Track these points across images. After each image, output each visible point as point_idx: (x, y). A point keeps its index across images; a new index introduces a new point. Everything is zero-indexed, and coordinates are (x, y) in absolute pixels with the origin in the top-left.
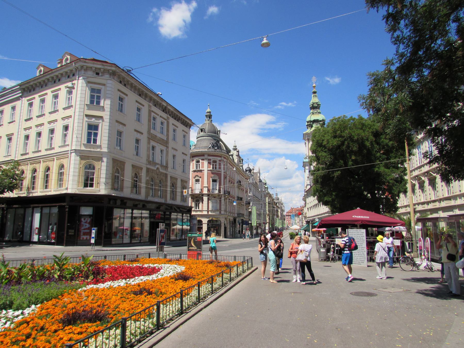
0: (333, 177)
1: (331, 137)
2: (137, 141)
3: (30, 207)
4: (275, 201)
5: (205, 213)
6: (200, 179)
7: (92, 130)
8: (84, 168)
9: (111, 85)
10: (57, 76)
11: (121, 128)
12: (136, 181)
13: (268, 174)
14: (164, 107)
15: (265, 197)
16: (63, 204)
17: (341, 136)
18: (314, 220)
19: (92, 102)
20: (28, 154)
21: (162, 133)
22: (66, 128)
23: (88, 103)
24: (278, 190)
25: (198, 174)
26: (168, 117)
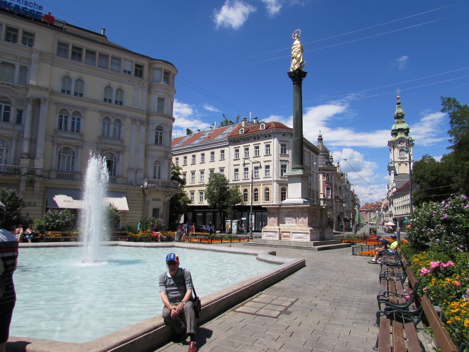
17: (436, 175)
19: (282, 152)
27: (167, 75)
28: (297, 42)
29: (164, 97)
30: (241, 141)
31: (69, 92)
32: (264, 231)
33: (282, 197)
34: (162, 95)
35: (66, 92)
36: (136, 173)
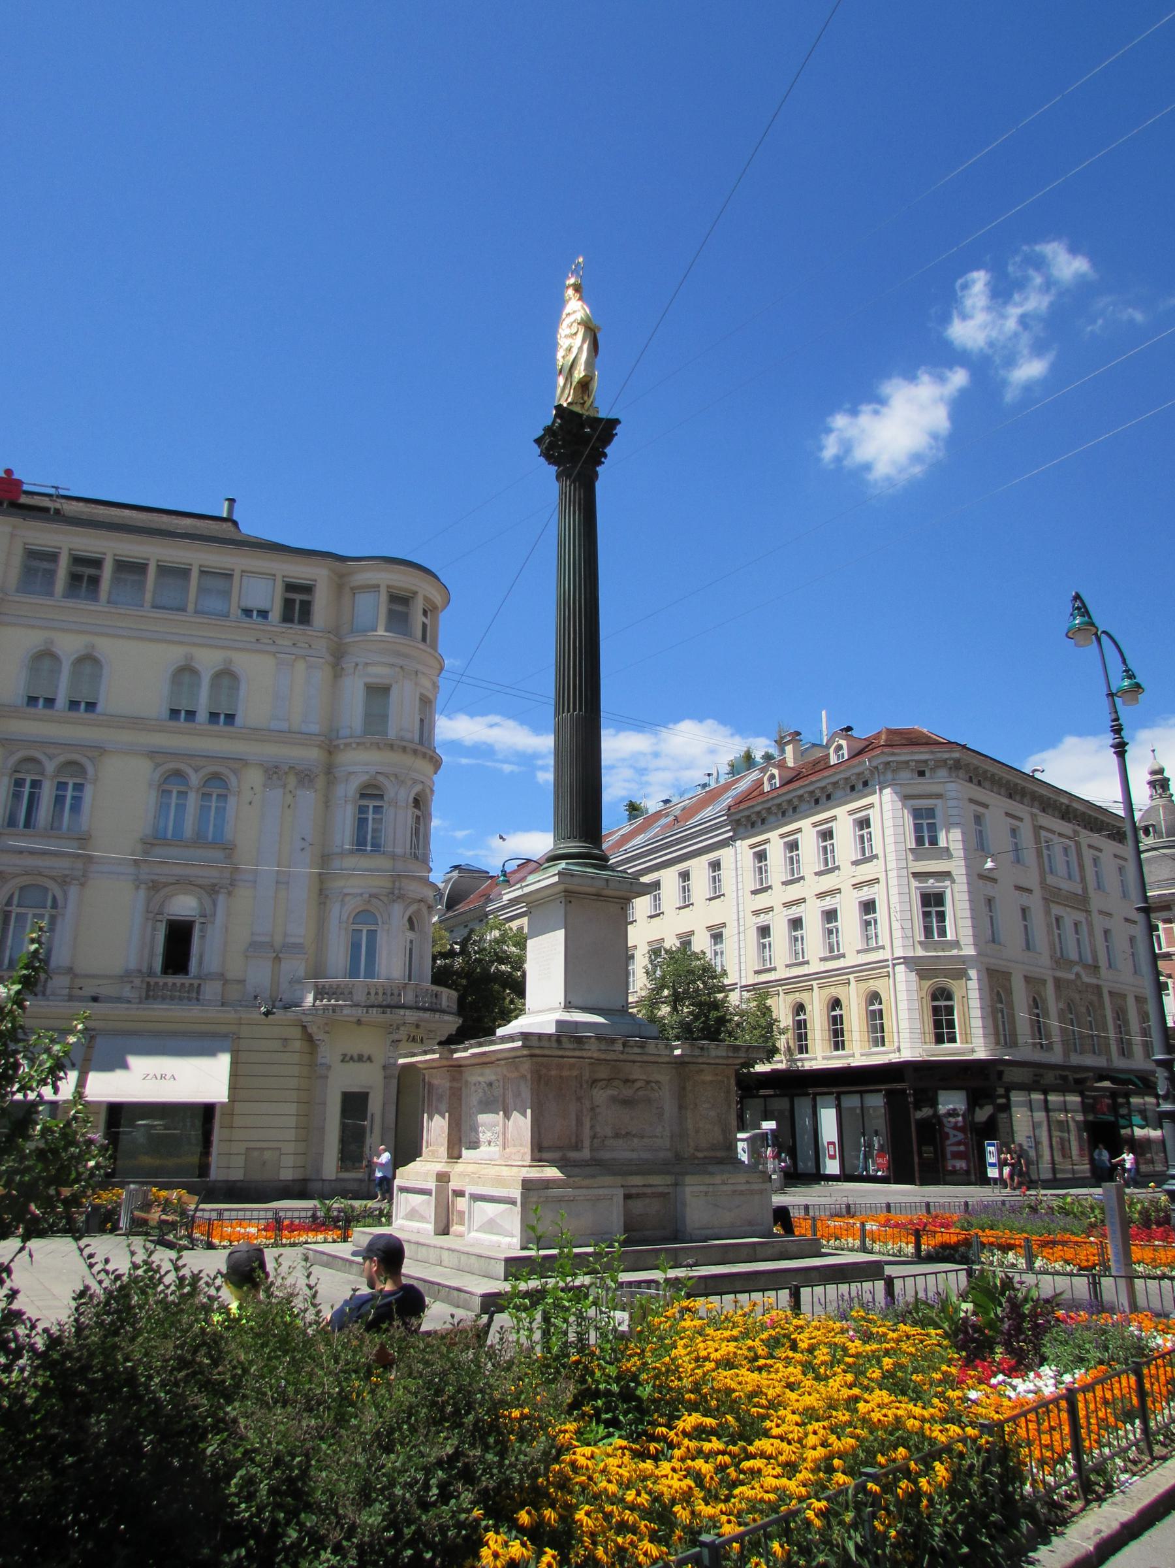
3: (809, 1095)
6: (1170, 981)
7: (932, 902)
8: (929, 998)
9: (956, 790)
10: (823, 789)
12: (1038, 1015)
16: (898, 1086)
19: (919, 841)
20: (774, 969)
22: (869, 907)
23: (914, 846)
26: (1075, 832)
27: (400, 601)
28: (575, 309)
29: (387, 681)
30: (772, 819)
31: (50, 702)
32: (403, 1189)
33: (937, 1024)
34: (379, 673)
35: (41, 701)
36: (277, 959)
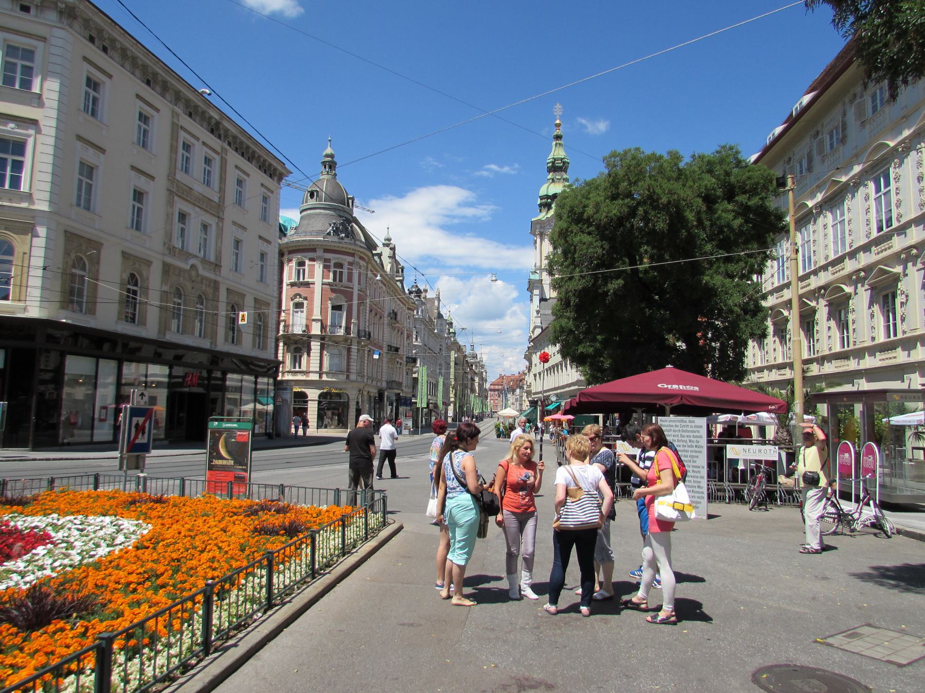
0: (606, 294)
1: (605, 199)
2: (139, 196)
4: (468, 359)
5: (314, 377)
6: (305, 302)
11: (91, 156)
13: (457, 306)
14: (213, 121)
15: (449, 349)
18: (547, 398)
21: (208, 184)
24: (476, 339)
25: (302, 291)
26: (222, 148)
